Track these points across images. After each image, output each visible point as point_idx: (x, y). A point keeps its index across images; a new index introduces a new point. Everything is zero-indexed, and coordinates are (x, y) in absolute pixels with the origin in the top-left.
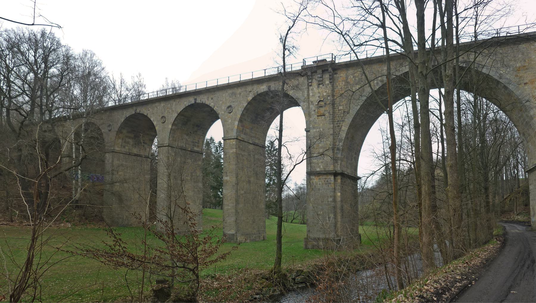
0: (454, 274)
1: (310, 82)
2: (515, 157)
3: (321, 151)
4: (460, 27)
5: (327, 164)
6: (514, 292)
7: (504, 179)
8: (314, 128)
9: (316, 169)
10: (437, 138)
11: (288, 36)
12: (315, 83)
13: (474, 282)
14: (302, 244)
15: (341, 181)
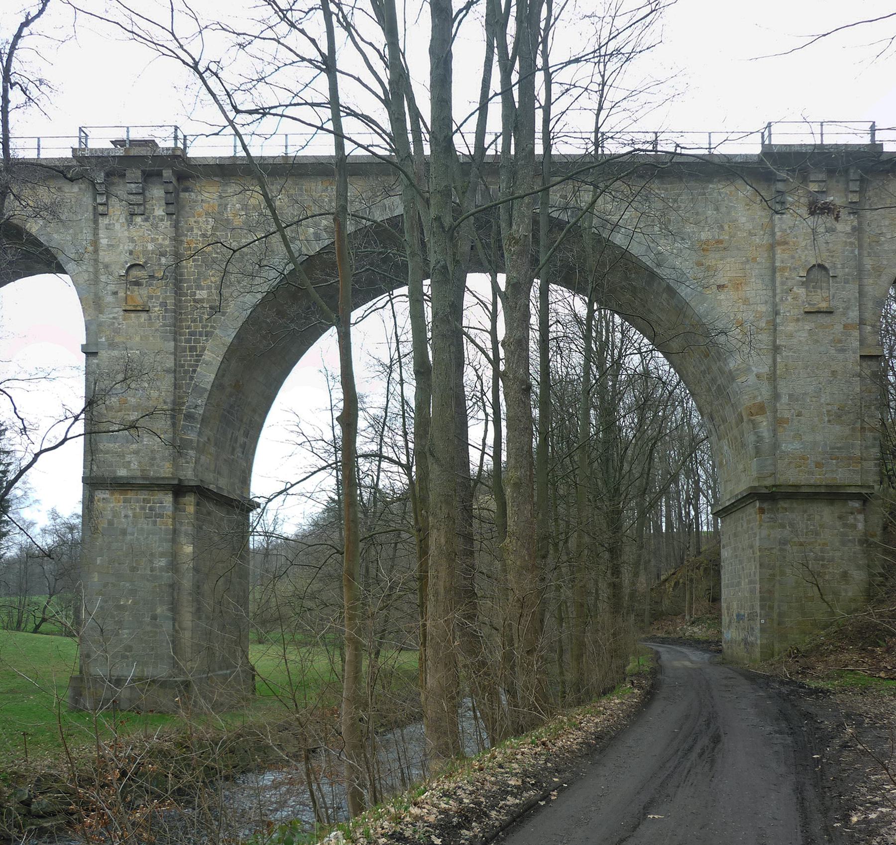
0: (502, 773)
1: (101, 204)
2: (691, 473)
3: (133, 416)
4: (555, 110)
5: (153, 459)
6: (656, 817)
7: (664, 531)
8: (112, 345)
9: (115, 472)
10: (485, 410)
11: (21, 43)
12: (117, 211)
13: (555, 793)
14: (66, 695)
15: (197, 512)
